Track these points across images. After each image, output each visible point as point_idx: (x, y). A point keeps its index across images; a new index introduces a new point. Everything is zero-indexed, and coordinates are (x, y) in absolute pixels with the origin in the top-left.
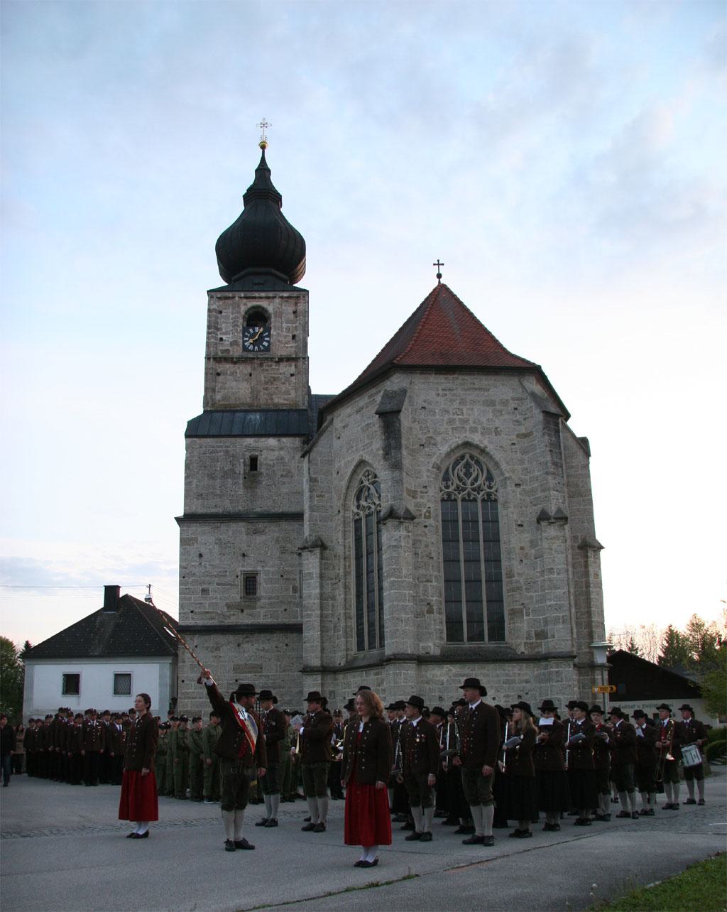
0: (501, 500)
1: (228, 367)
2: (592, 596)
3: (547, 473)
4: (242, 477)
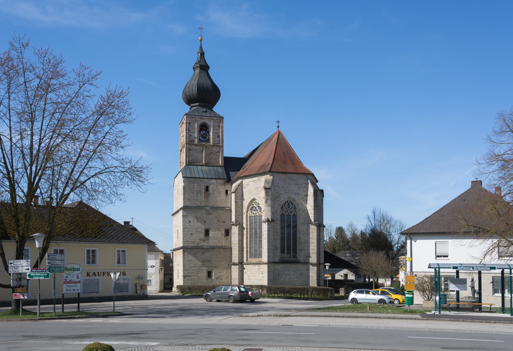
0: (298, 215)
4: (203, 193)
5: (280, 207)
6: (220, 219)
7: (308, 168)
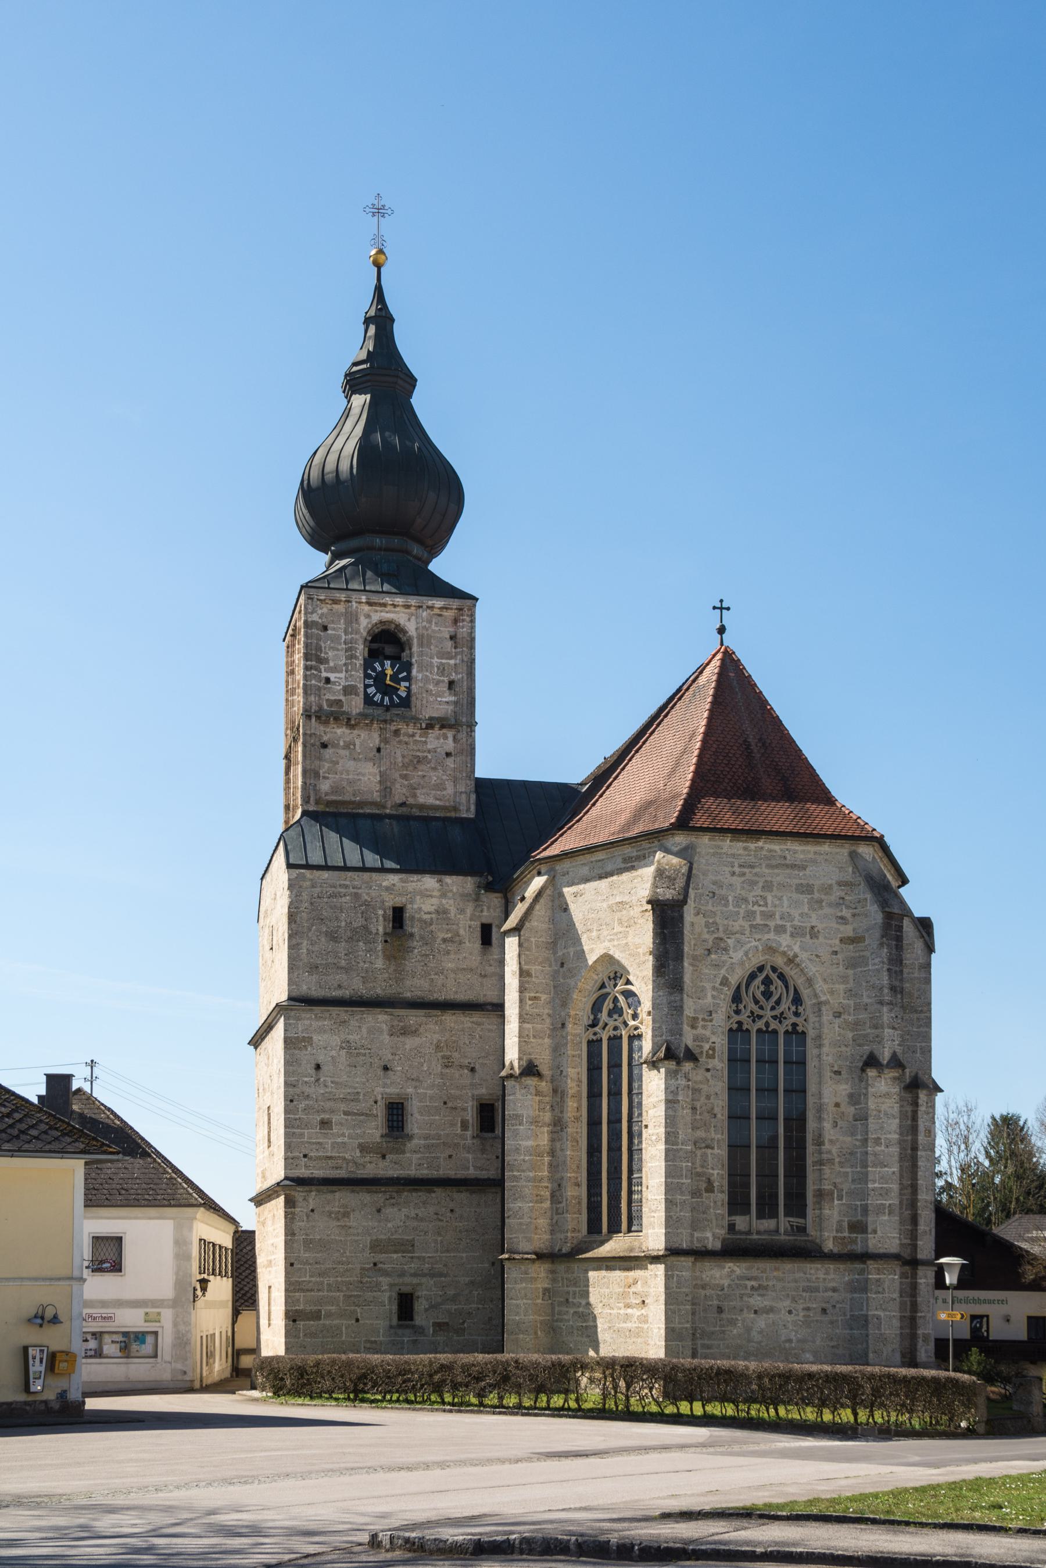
0: (811, 1033)
1: (340, 732)
2: (920, 1163)
3: (881, 1003)
4: (380, 939)
5: (728, 992)
6: (456, 1055)
7: (857, 812)
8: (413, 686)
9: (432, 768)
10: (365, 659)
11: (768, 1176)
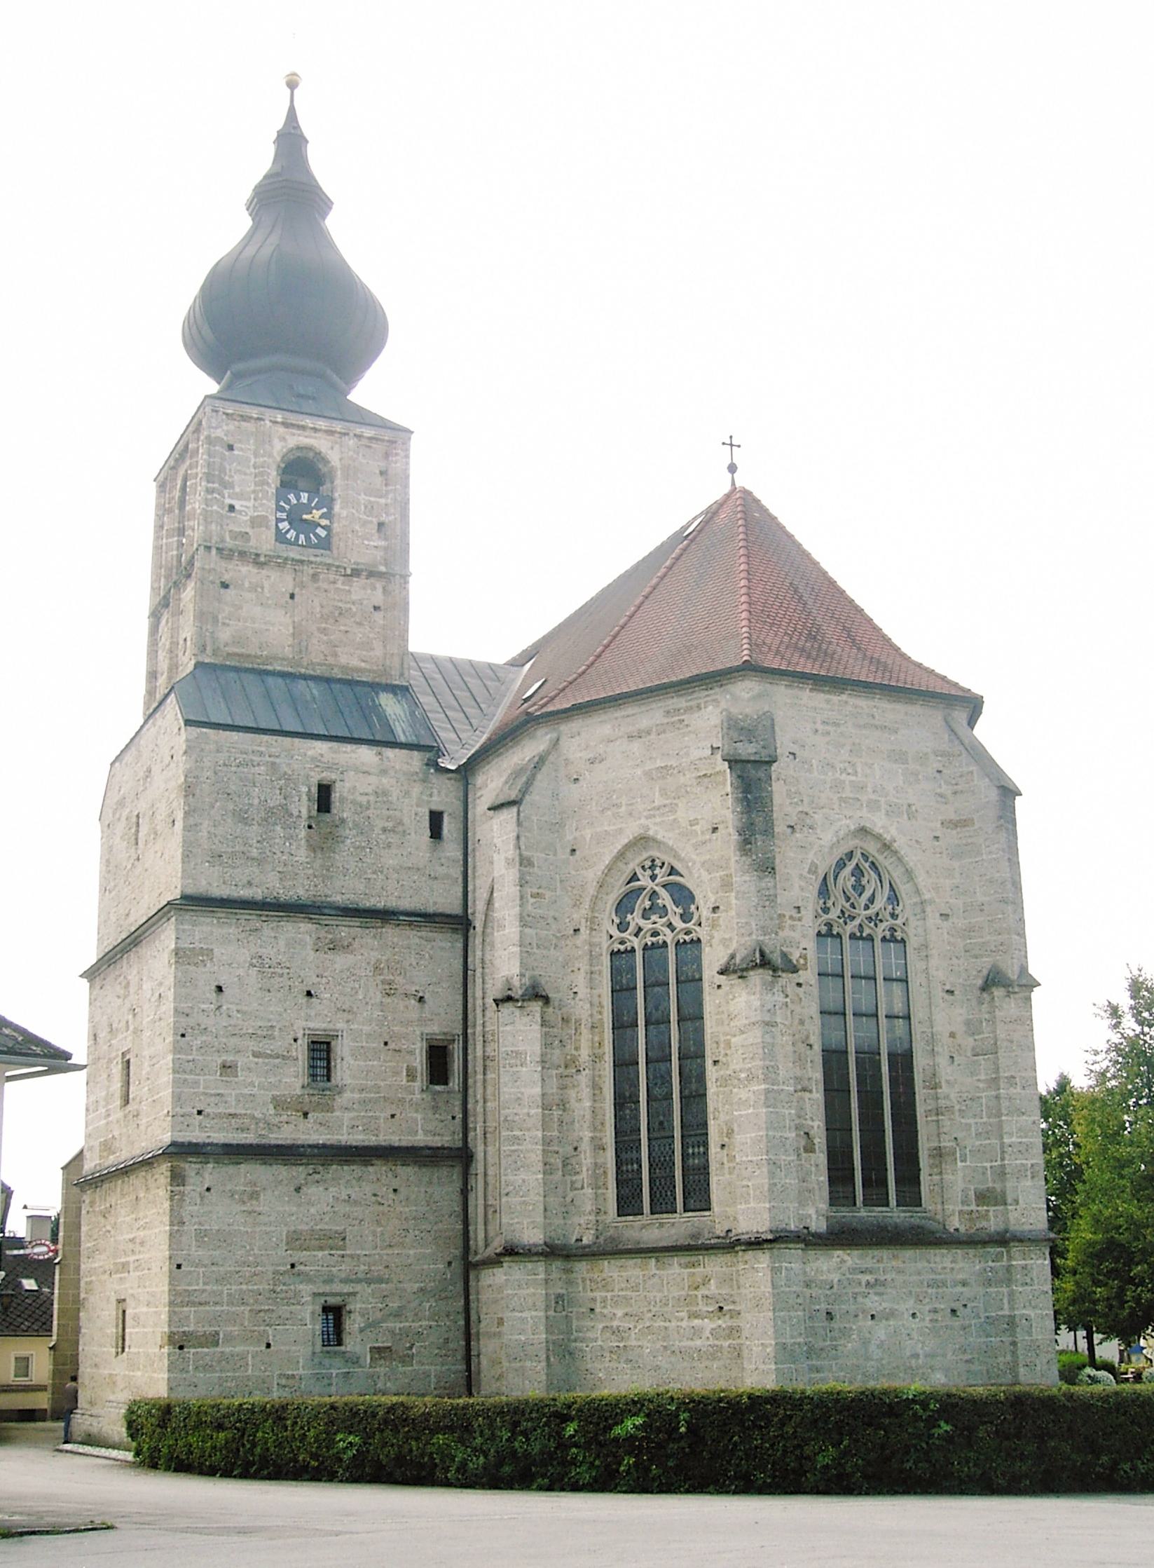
4: (305, 823)
6: (399, 979)
8: (335, 525)
9: (357, 623)
10: (277, 489)
11: (661, 1164)
